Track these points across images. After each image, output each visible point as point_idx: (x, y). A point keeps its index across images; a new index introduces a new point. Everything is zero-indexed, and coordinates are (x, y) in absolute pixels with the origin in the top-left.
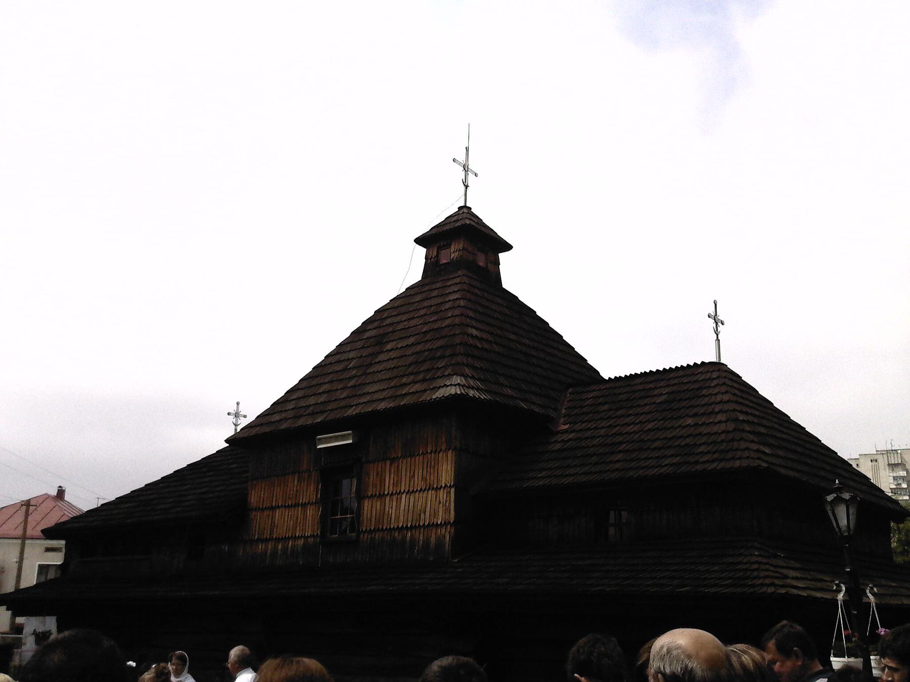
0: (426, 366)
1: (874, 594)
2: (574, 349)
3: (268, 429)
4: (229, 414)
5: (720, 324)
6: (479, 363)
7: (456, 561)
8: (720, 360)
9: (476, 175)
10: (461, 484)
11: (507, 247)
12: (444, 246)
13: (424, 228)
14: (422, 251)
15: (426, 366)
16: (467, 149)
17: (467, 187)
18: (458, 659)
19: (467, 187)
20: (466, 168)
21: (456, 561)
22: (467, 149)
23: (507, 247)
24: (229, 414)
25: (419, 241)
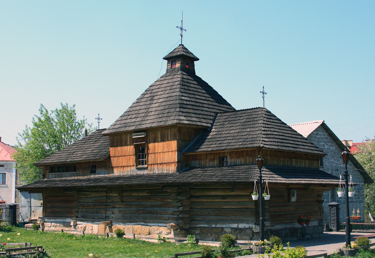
0: (166, 111)
1: (351, 176)
2: (222, 97)
3: (114, 131)
4: (96, 119)
5: (265, 94)
6: (155, 198)
7: (178, 173)
8: (264, 107)
9: (186, 30)
10: (179, 150)
11: (198, 59)
12: (174, 61)
13: (166, 54)
14: (166, 61)
15: (166, 111)
16: (182, 21)
17: (182, 36)
18: (325, 203)
19: (182, 36)
20: (181, 29)
21: (178, 173)
22: (182, 21)
23: (198, 59)
24: (96, 119)
25: (164, 59)
